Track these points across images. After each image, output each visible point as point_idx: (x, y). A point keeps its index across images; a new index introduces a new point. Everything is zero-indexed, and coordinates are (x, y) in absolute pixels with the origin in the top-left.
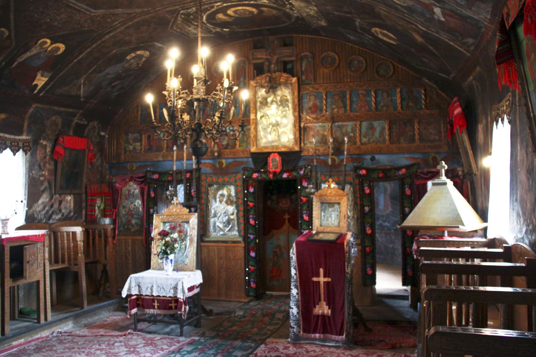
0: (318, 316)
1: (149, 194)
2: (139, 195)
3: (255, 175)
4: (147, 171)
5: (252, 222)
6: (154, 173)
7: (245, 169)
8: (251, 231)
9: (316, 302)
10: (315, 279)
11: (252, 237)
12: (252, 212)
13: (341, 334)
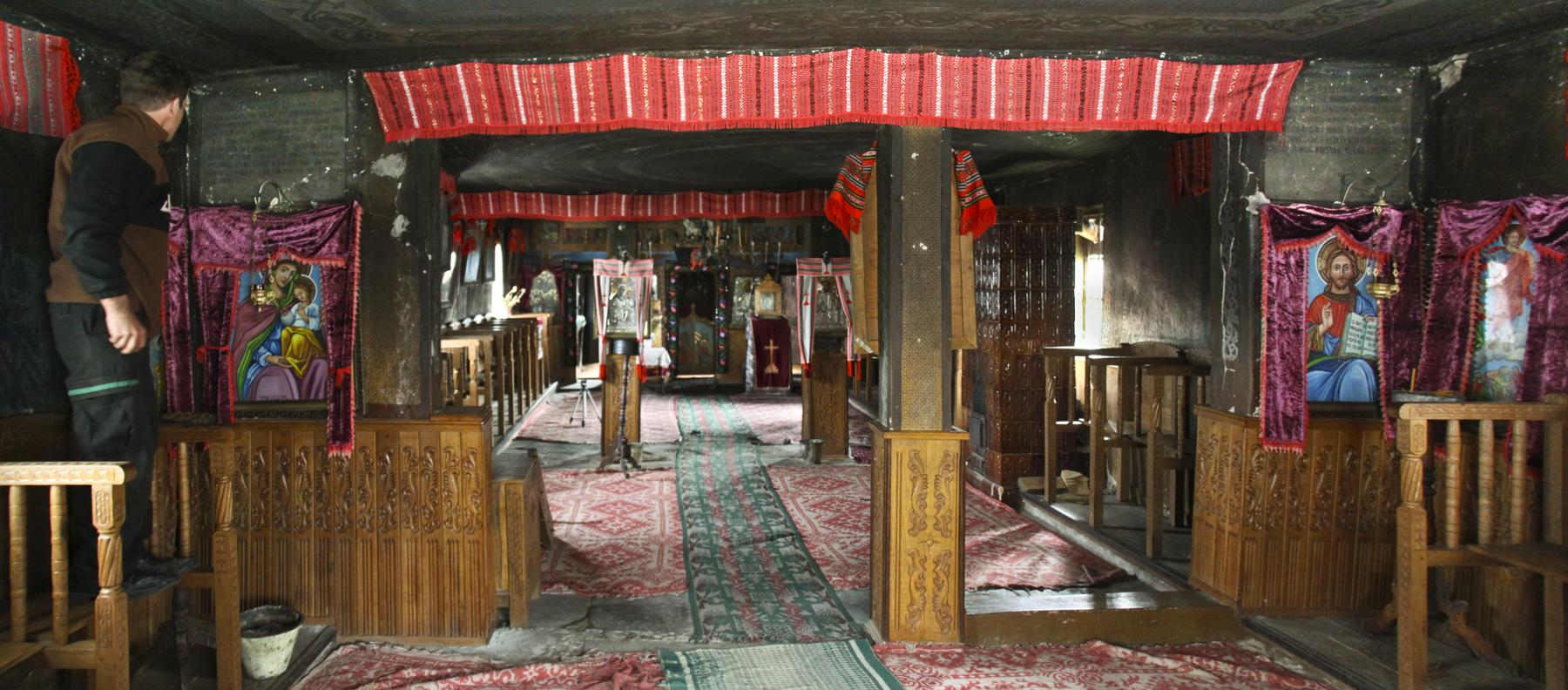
0: (768, 375)
1: (567, 285)
2: (554, 285)
3: (677, 268)
4: (565, 261)
5: (673, 310)
6: (573, 263)
7: (668, 262)
8: (672, 318)
9: (768, 364)
10: (767, 348)
11: (673, 323)
12: (673, 301)
13: (787, 386)
